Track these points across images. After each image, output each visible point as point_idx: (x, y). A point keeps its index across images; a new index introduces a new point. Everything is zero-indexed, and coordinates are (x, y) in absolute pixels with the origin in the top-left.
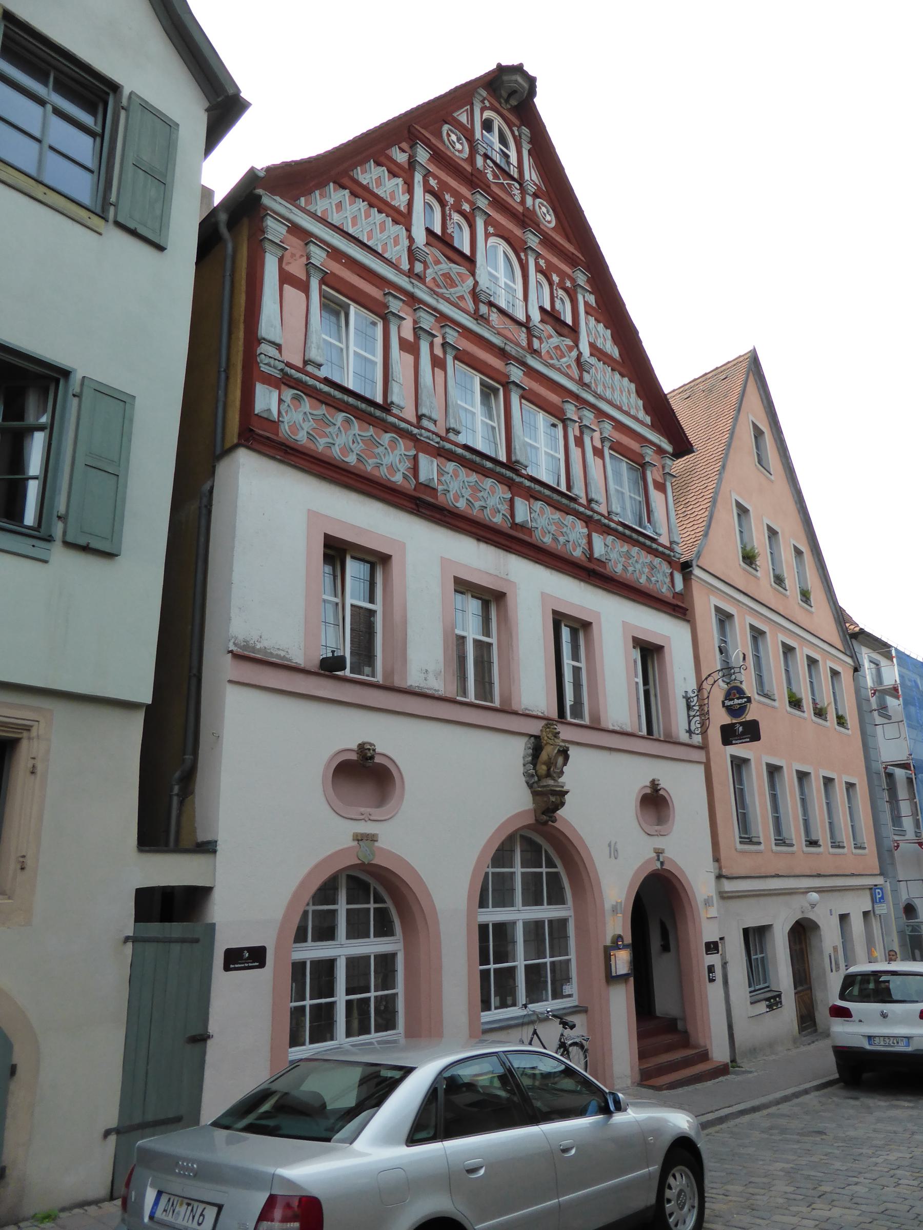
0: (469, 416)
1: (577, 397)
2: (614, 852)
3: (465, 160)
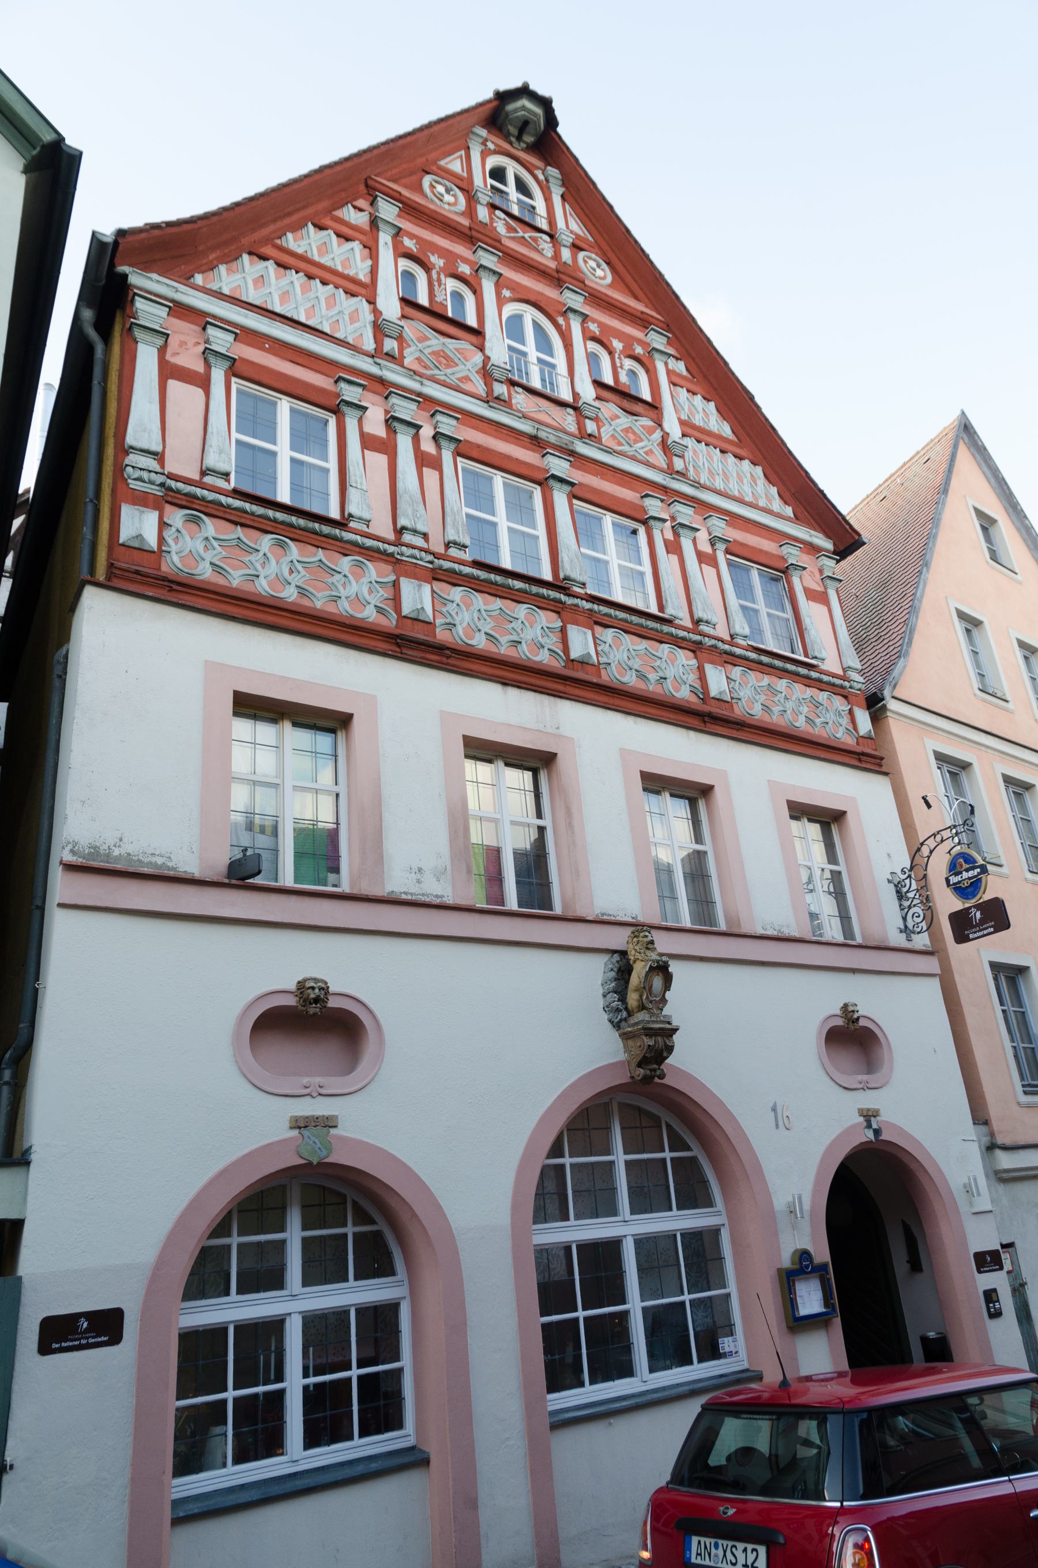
3: (463, 214)
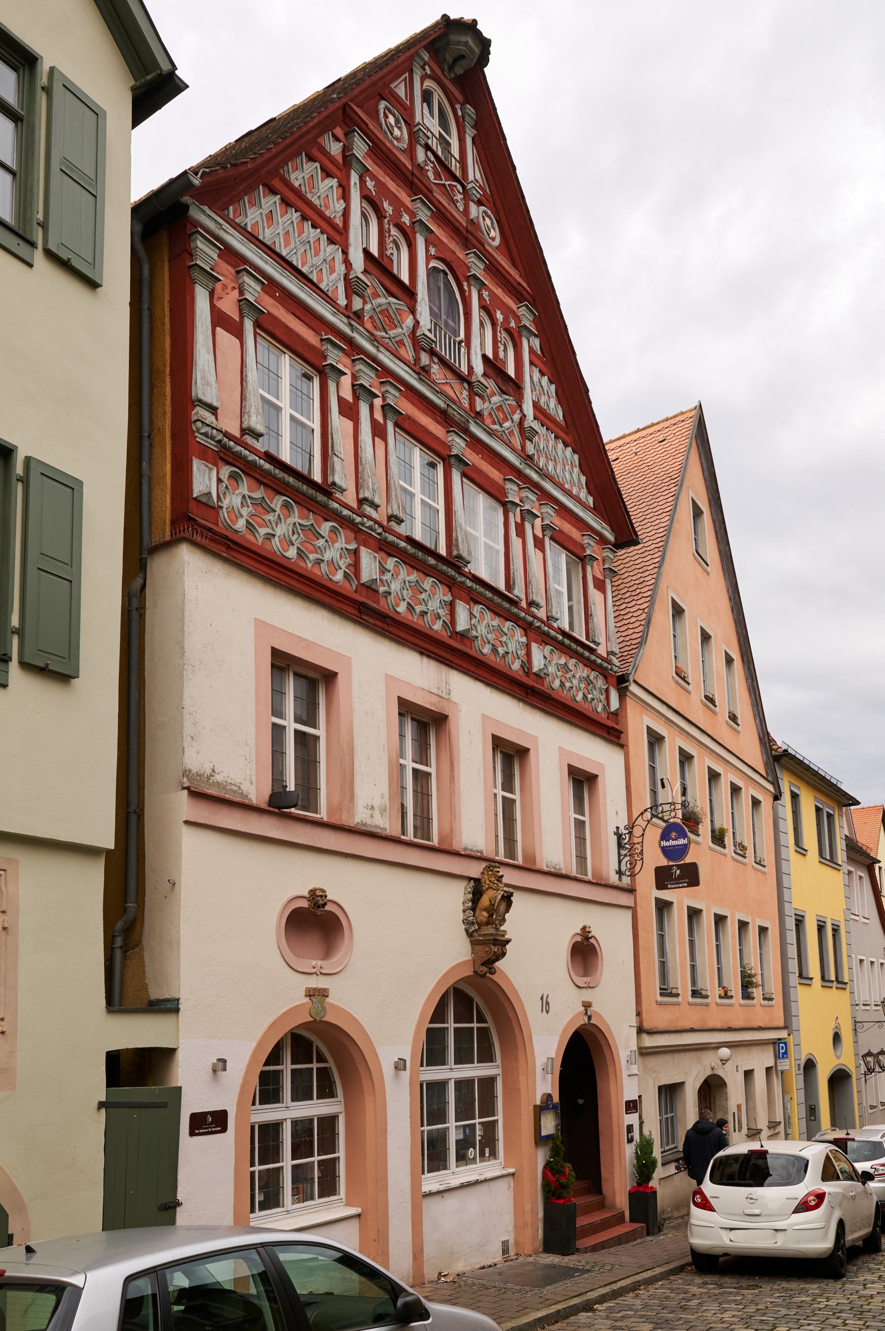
0: (408, 497)
1: (519, 473)
2: (546, 1005)
